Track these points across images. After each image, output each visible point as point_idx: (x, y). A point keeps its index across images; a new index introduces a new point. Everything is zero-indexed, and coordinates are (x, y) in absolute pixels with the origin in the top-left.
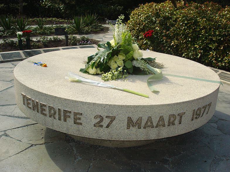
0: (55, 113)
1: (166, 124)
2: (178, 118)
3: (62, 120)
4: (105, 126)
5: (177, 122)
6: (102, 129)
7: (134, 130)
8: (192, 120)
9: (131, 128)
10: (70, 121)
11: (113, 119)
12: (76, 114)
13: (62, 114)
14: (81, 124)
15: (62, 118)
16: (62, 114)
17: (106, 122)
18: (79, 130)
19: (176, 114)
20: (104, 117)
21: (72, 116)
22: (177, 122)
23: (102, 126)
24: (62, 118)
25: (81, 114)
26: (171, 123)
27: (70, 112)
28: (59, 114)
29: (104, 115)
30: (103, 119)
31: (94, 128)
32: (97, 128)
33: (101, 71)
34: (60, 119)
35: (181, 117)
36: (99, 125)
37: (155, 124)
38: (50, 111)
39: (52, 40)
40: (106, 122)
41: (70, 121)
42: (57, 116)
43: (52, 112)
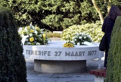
0: (41, 53)
1: (79, 55)
2: (82, 53)
3: (44, 52)
4: (58, 55)
5: (82, 55)
6: (57, 56)
7: (67, 56)
8: (88, 55)
9: (67, 56)
10: (47, 55)
11: (61, 53)
12: (49, 52)
13: (44, 53)
14: (50, 55)
15: (44, 54)
16: (44, 53)
17: (59, 54)
18: (49, 58)
19: (82, 52)
20: (58, 52)
21: (47, 53)
22: (82, 55)
23: (57, 55)
24: (44, 54)
25: (50, 52)
26: (80, 55)
27: (46, 52)
28: (43, 53)
29: (58, 51)
30: (57, 53)
31: (54, 56)
32: (55, 56)
33: (49, 26)
34: (43, 55)
35: (83, 53)
36: (56, 55)
37: (74, 55)
38: (39, 53)
39: (35, 12)
40: (59, 54)
41: (47, 55)
42: (42, 54)
43: (40, 53)
